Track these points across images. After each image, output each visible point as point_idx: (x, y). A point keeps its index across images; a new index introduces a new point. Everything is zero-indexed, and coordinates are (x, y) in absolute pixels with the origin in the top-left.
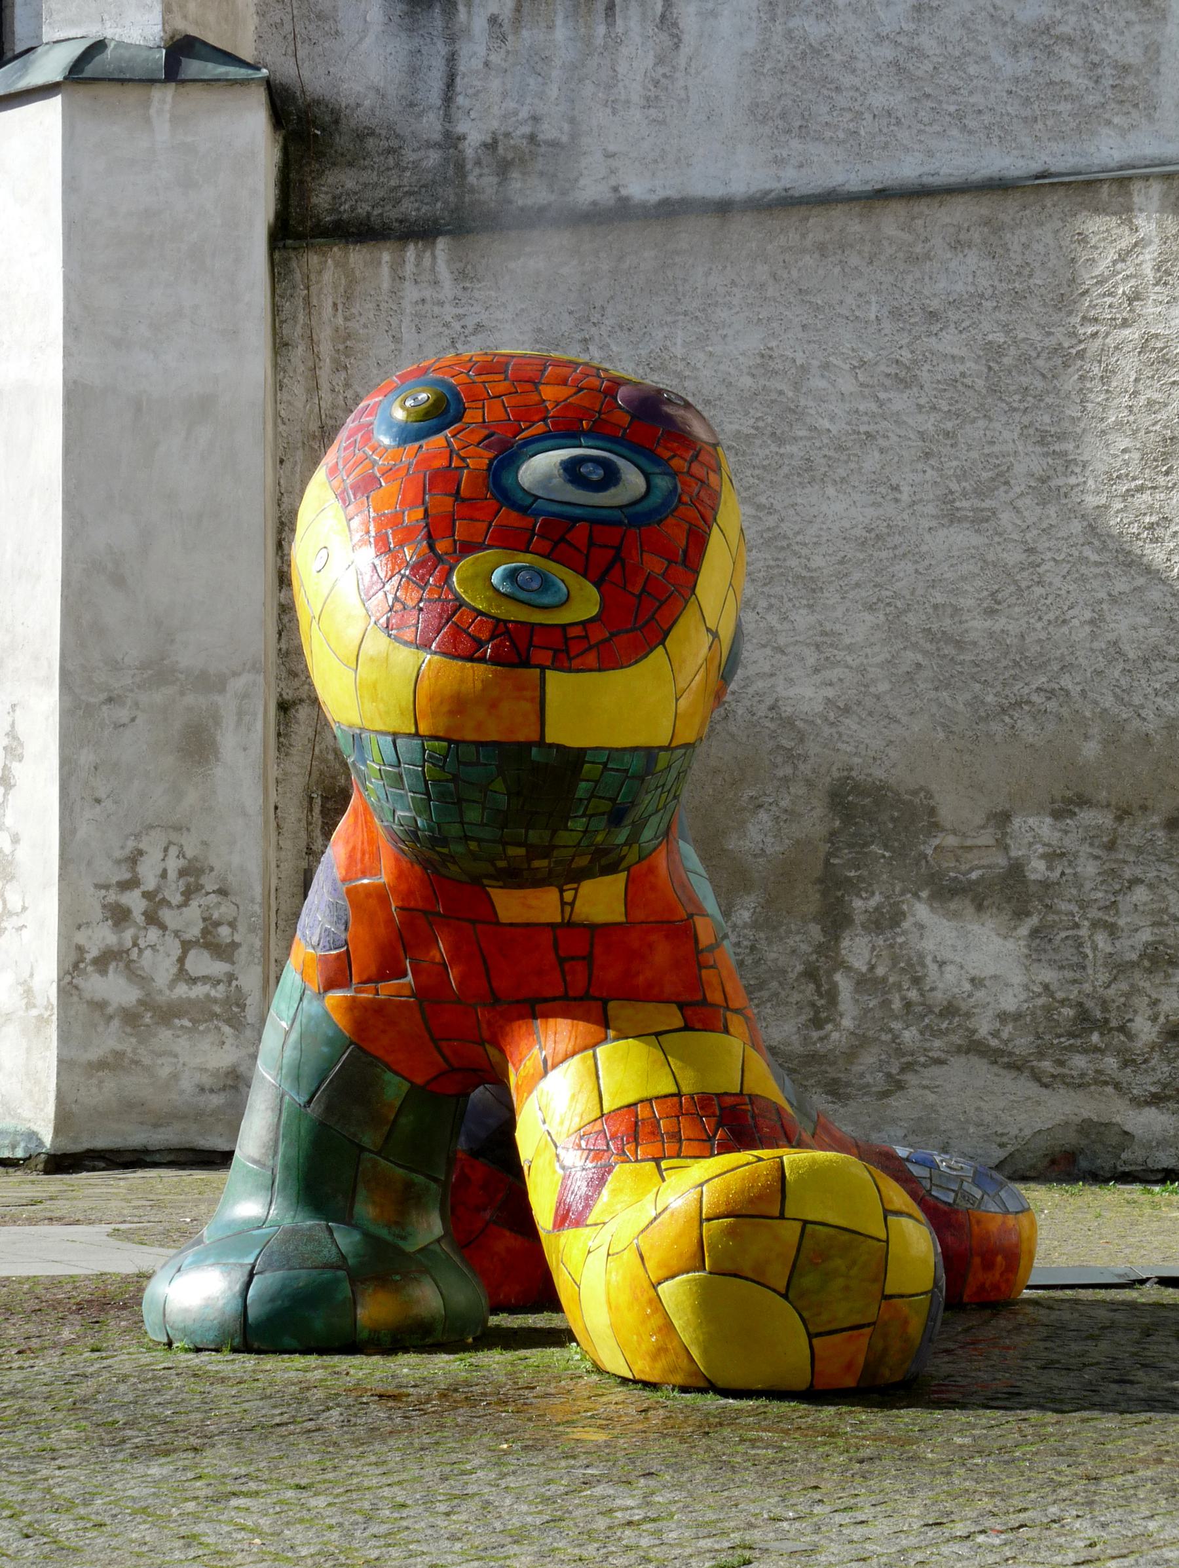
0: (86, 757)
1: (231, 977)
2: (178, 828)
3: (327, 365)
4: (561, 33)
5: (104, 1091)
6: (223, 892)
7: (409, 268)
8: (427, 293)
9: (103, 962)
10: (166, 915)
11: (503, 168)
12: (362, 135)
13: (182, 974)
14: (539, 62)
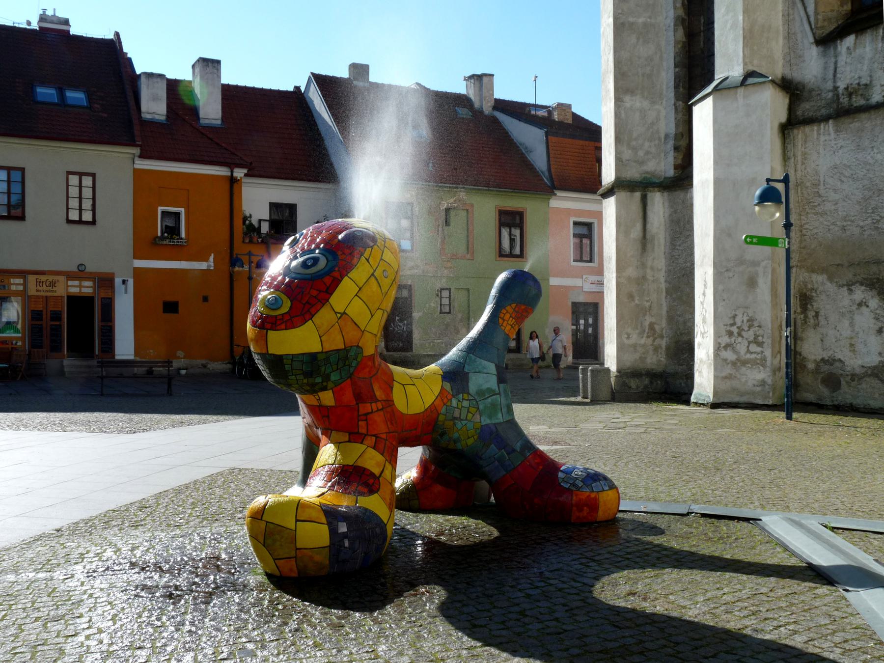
0: (721, 287)
1: (762, 352)
2: (747, 308)
3: (800, 163)
4: (868, 49)
5: (726, 385)
6: (760, 326)
7: (822, 130)
8: (827, 138)
9: (726, 347)
10: (744, 333)
11: (850, 95)
12: (811, 91)
13: (748, 351)
14: (861, 59)
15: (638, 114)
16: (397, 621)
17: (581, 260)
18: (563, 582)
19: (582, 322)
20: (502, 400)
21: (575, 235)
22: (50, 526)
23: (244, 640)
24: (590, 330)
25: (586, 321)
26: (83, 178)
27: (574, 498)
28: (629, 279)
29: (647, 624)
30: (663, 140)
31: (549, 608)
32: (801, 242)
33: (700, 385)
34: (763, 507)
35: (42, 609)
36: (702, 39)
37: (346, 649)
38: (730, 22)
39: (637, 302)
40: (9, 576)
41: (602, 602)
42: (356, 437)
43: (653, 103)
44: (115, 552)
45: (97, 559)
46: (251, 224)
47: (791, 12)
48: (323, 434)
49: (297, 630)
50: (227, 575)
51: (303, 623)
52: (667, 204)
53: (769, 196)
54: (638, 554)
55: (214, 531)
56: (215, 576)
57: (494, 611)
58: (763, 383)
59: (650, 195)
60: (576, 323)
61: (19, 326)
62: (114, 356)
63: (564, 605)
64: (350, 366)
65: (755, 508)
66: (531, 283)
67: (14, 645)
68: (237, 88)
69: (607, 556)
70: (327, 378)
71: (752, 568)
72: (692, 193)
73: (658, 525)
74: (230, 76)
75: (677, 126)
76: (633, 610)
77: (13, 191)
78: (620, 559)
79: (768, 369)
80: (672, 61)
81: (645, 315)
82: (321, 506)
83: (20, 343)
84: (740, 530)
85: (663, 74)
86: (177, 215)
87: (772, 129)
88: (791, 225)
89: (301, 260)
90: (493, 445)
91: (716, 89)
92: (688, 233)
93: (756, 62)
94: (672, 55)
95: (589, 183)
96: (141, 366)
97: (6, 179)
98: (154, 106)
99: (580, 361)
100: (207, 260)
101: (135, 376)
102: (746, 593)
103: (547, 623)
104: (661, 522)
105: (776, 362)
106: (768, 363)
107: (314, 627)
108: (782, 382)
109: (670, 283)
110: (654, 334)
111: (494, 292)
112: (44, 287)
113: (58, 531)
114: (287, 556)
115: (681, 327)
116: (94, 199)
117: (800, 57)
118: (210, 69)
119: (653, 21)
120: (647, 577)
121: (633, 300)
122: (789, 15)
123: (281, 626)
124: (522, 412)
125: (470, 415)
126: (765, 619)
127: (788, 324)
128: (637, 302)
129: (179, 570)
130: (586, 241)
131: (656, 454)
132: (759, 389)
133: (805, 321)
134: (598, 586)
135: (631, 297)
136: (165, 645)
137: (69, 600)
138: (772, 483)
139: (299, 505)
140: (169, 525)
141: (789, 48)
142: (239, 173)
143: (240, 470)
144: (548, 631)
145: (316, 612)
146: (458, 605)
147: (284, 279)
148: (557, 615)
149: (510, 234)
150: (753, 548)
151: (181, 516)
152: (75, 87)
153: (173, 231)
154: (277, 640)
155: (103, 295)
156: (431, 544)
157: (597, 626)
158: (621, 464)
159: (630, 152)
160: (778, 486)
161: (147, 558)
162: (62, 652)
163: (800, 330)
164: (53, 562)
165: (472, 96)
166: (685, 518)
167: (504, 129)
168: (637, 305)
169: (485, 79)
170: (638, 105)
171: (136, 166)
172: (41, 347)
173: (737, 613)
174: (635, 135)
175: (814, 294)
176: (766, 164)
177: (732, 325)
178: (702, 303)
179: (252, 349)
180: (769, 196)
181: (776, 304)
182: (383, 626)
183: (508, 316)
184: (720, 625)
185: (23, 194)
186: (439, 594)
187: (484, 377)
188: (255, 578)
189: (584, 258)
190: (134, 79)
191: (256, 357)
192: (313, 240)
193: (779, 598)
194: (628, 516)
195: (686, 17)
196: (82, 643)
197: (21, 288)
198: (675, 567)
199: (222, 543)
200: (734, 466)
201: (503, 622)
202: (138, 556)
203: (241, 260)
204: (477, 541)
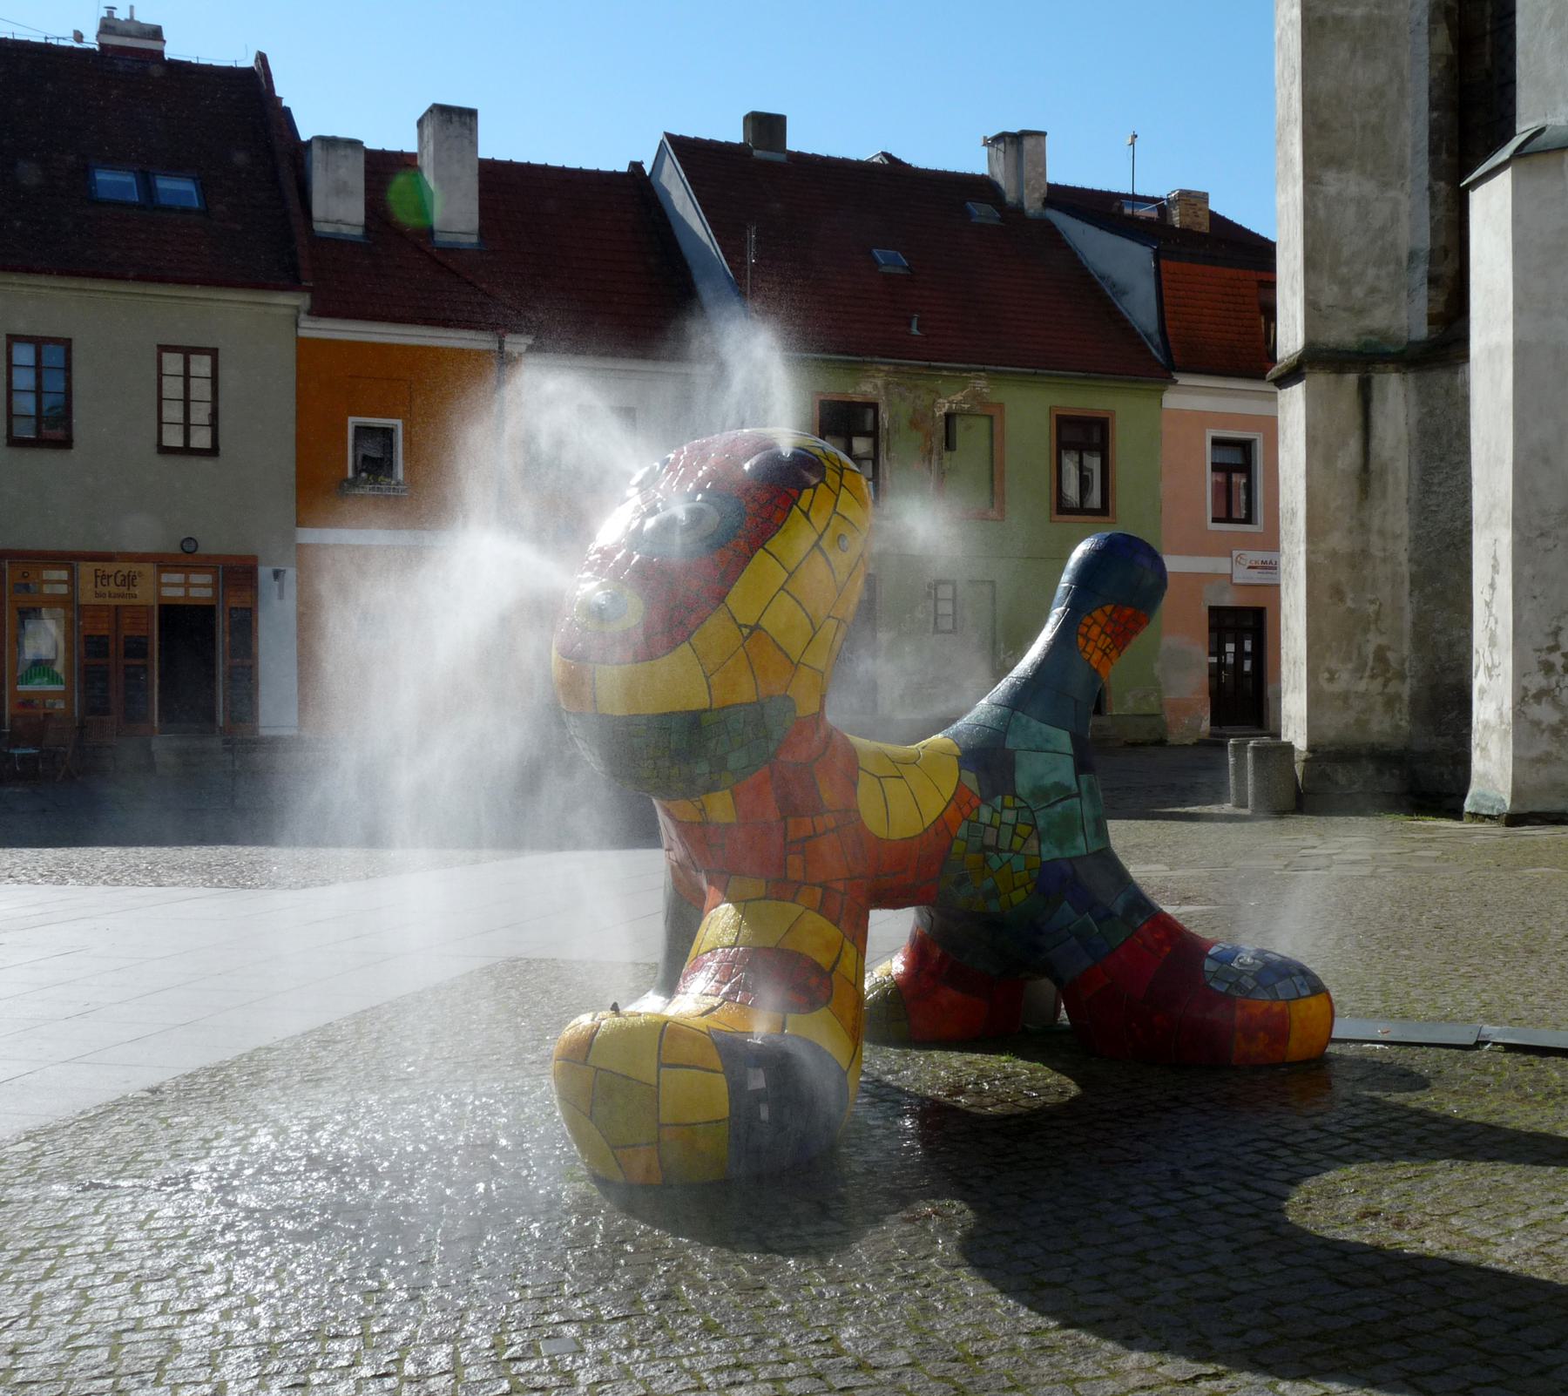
0: (1528, 571)
9: (1539, 696)
15: (1351, 211)
17: (1229, 519)
18: (1224, 1191)
19: (1230, 647)
20: (1084, 808)
21: (1216, 467)
22: (138, 1082)
23: (556, 1317)
24: (1247, 666)
26: (193, 358)
27: (1238, 1013)
28: (1333, 555)
29: (1407, 1277)
30: (1405, 264)
33: (1484, 776)
37: (773, 1335)
39: (1349, 603)
40: (54, 1187)
41: (1305, 1233)
43: (1385, 185)
44: (276, 1137)
45: (237, 1149)
48: (710, 883)
49: (666, 1297)
52: (1413, 397)
54: (1377, 1131)
55: (481, 1089)
59: (1377, 379)
60: (1217, 650)
61: (59, 668)
67: (72, 1330)
68: (510, 166)
69: (1311, 1135)
73: (1416, 1069)
74: (494, 144)
75: (1434, 232)
76: (1376, 1250)
77: (47, 386)
78: (1340, 1141)
81: (1366, 631)
82: (710, 1033)
83: (61, 705)
85: (1406, 125)
86: (388, 433)
90: (1066, 905)
91: (1519, 154)
94: (1424, 84)
95: (1247, 355)
97: (32, 363)
98: (338, 207)
99: (1226, 730)
103: (1195, 1277)
104: (1422, 1062)
107: (700, 1287)
109: (1419, 564)
111: (1065, 580)
112: (113, 588)
113: (153, 1091)
121: (1342, 600)
124: (1123, 835)
128: (1349, 603)
129: (412, 1171)
130: (1239, 480)
131: (1400, 920)
134: (1297, 1197)
135: (1338, 593)
136: (388, 1331)
137: (183, 1236)
147: (629, 557)
149: (1081, 468)
152: (175, 169)
154: (626, 1317)
155: (234, 602)
159: (1336, 289)
161: (344, 1147)
162: (174, 1346)
164: (147, 1156)
165: (1000, 179)
166: (1471, 1054)
167: (1068, 247)
168: (1351, 611)
169: (1028, 143)
170: (1353, 190)
171: (303, 333)
174: (1346, 252)
177: (1552, 649)
178: (1488, 604)
182: (847, 1287)
183: (1096, 630)
185: (68, 393)
187: (1047, 761)
189: (1235, 515)
190: (299, 152)
194: (1350, 1050)
196: (215, 1326)
197: (63, 589)
198: (1457, 1157)
199: (499, 1114)
204: (1036, 1105)
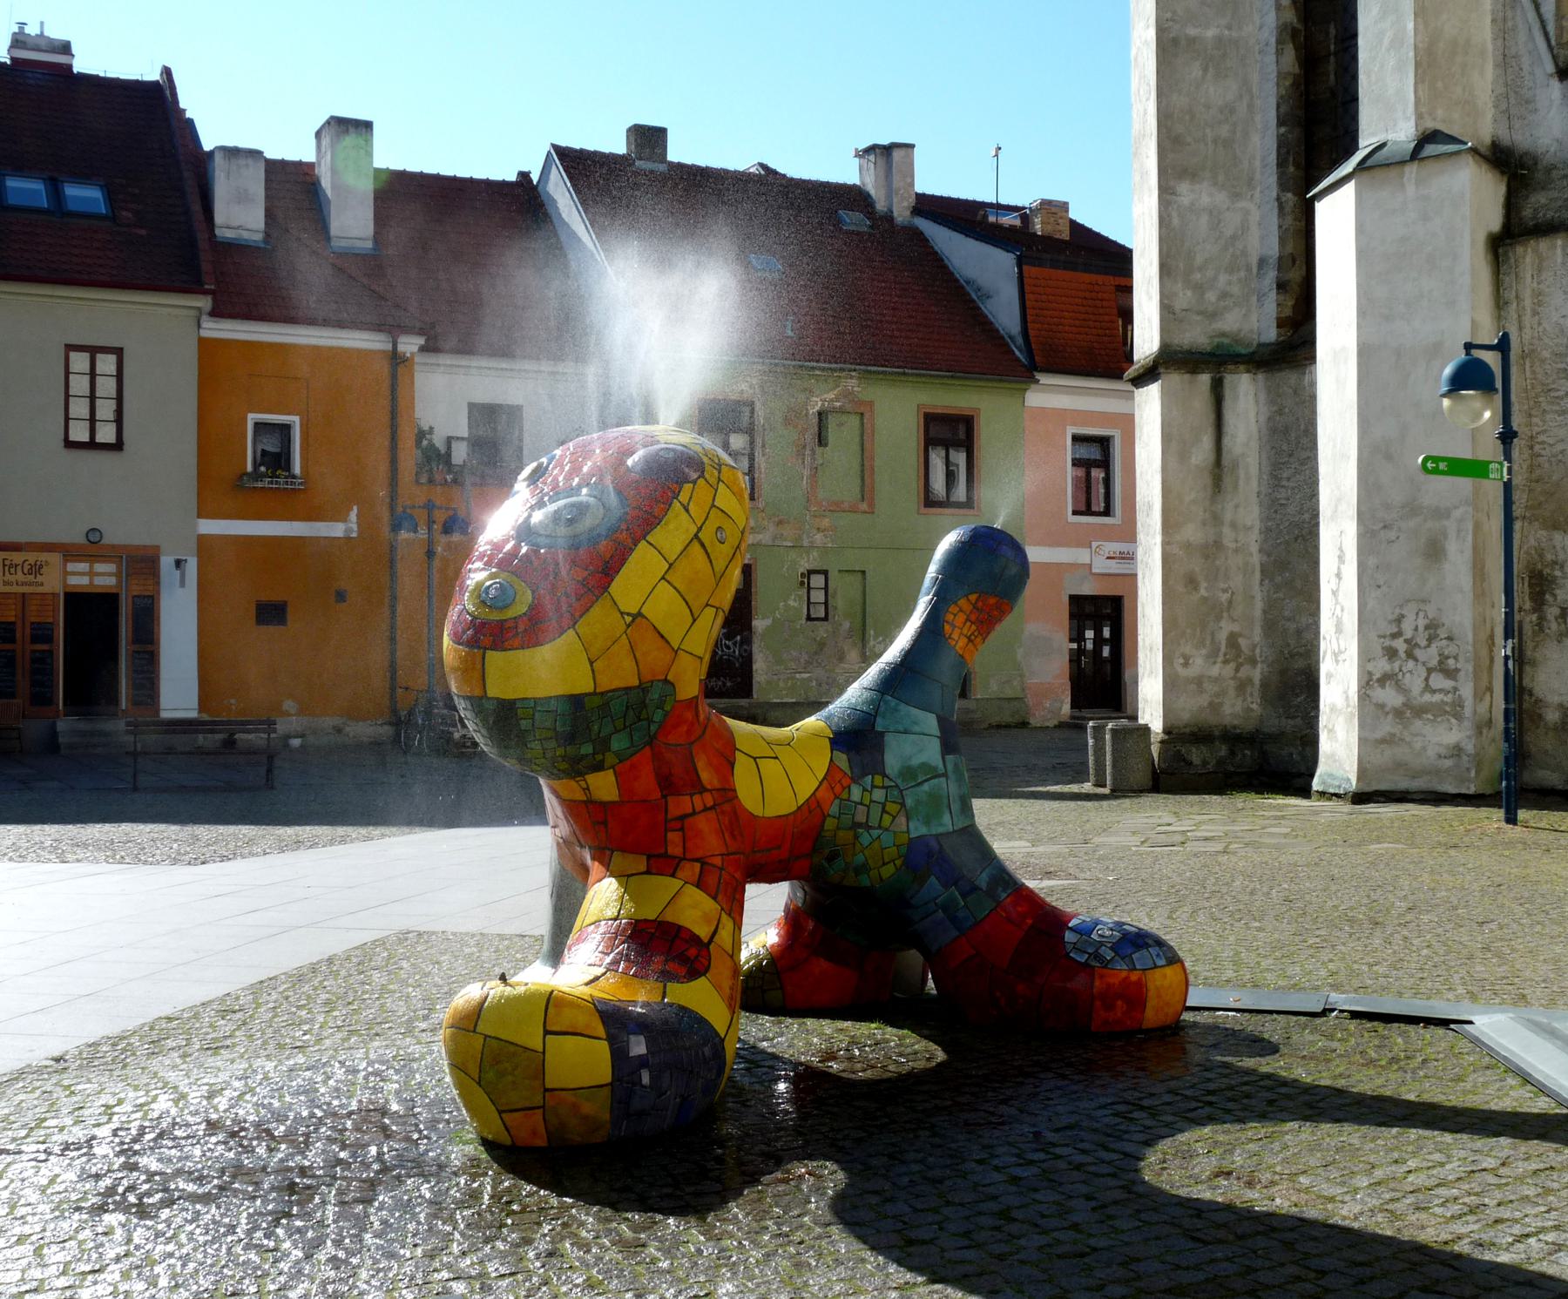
0: (1372, 561)
1: (1456, 689)
2: (1424, 601)
3: (1529, 311)
6: (1450, 638)
9: (1384, 680)
10: (1417, 652)
12: (1551, 168)
15: (1204, 219)
16: (754, 1234)
17: (1088, 511)
18: (1083, 1152)
19: (1090, 634)
21: (1076, 463)
23: (445, 1275)
24: (1106, 651)
25: (1098, 633)
27: (1097, 983)
28: (1188, 546)
29: (1258, 1233)
30: (1255, 270)
31: (1059, 1204)
32: (1531, 469)
33: (1332, 756)
34: (1473, 997)
35: (29, 1218)
36: (1331, 67)
38: (1389, 35)
39: (1203, 592)
41: (1161, 1192)
42: (662, 864)
43: (1236, 196)
44: (176, 1102)
45: (139, 1115)
46: (432, 446)
47: (1509, 14)
48: (593, 859)
49: (550, 1254)
50: (403, 1145)
51: (563, 1239)
52: (1262, 396)
53: (1470, 377)
54: (1229, 1094)
55: (372, 1056)
56: (380, 1146)
57: (946, 1211)
58: (1457, 751)
59: (1229, 379)
60: (1078, 637)
62: (157, 711)
63: (1089, 1198)
64: (650, 721)
65: (1458, 999)
66: (1010, 553)
69: (1167, 1098)
70: (603, 745)
71: (1461, 1119)
72: (1313, 374)
73: (1266, 1036)
75: (1282, 241)
76: (1228, 1208)
78: (1194, 1104)
79: (1466, 723)
80: (1274, 113)
81: (1219, 618)
84: (1430, 1044)
85: (1256, 139)
86: (285, 429)
87: (1473, 242)
88: (1515, 434)
89: (552, 508)
90: (933, 879)
92: (1304, 455)
93: (1440, 113)
95: (1106, 357)
96: (212, 732)
98: (239, 213)
99: (1086, 713)
100: (345, 520)
101: (201, 752)
102: (1452, 1169)
103: (1055, 1234)
104: (1271, 1030)
105: (1483, 708)
106: (1468, 712)
107: (585, 1246)
108: (1496, 749)
109: (1269, 555)
110: (1238, 656)
111: (933, 570)
112: (20, 577)
113: (57, 1060)
114: (528, 1104)
115: (1292, 642)
116: (119, 399)
117: (1527, 102)
118: (350, 140)
119: (1234, 34)
120: (1251, 1140)
121: (1196, 589)
122: (1505, 20)
123: (518, 1246)
124: (988, 813)
125: (887, 819)
126: (1496, 1221)
127: (1508, 634)
128: (1203, 592)
129: (307, 1135)
130: (1098, 474)
131: (1252, 893)
132: (1448, 763)
133: (1540, 625)
134: (1152, 1157)
135: (1192, 582)
138: (1487, 949)
139: (551, 1001)
140: (281, 1047)
141: (1507, 85)
142: (409, 345)
143: (420, 934)
144: (1060, 1250)
145: (588, 1219)
146: (874, 1200)
147: (517, 548)
148: (1076, 1218)
150: (1459, 1079)
151: (306, 1027)
152: (83, 177)
153: (277, 461)
154: (512, 1274)
155: (136, 590)
156: (809, 1080)
157: (1157, 1238)
158: (1183, 913)
160: (1499, 955)
161: (241, 1112)
163: (1529, 645)
166: (1318, 1021)
168: (1205, 599)
170: (1205, 200)
171: (204, 333)
172: (13, 696)
173: (1438, 1210)
174: (1199, 260)
175: (1558, 573)
176: (1461, 315)
178: (1334, 593)
179: (454, 690)
180: (1470, 377)
181: (1483, 594)
183: (961, 618)
184: (1406, 1236)
186: (833, 1177)
187: (915, 743)
188: (463, 1149)
189: (1094, 508)
190: (201, 162)
191: (461, 705)
192: (576, 469)
193: (1520, 1179)
195: (1300, 26)
198: (1306, 1119)
200: (1408, 918)
201: (967, 1234)
202: (222, 1108)
203: (411, 516)
204: (905, 1070)
